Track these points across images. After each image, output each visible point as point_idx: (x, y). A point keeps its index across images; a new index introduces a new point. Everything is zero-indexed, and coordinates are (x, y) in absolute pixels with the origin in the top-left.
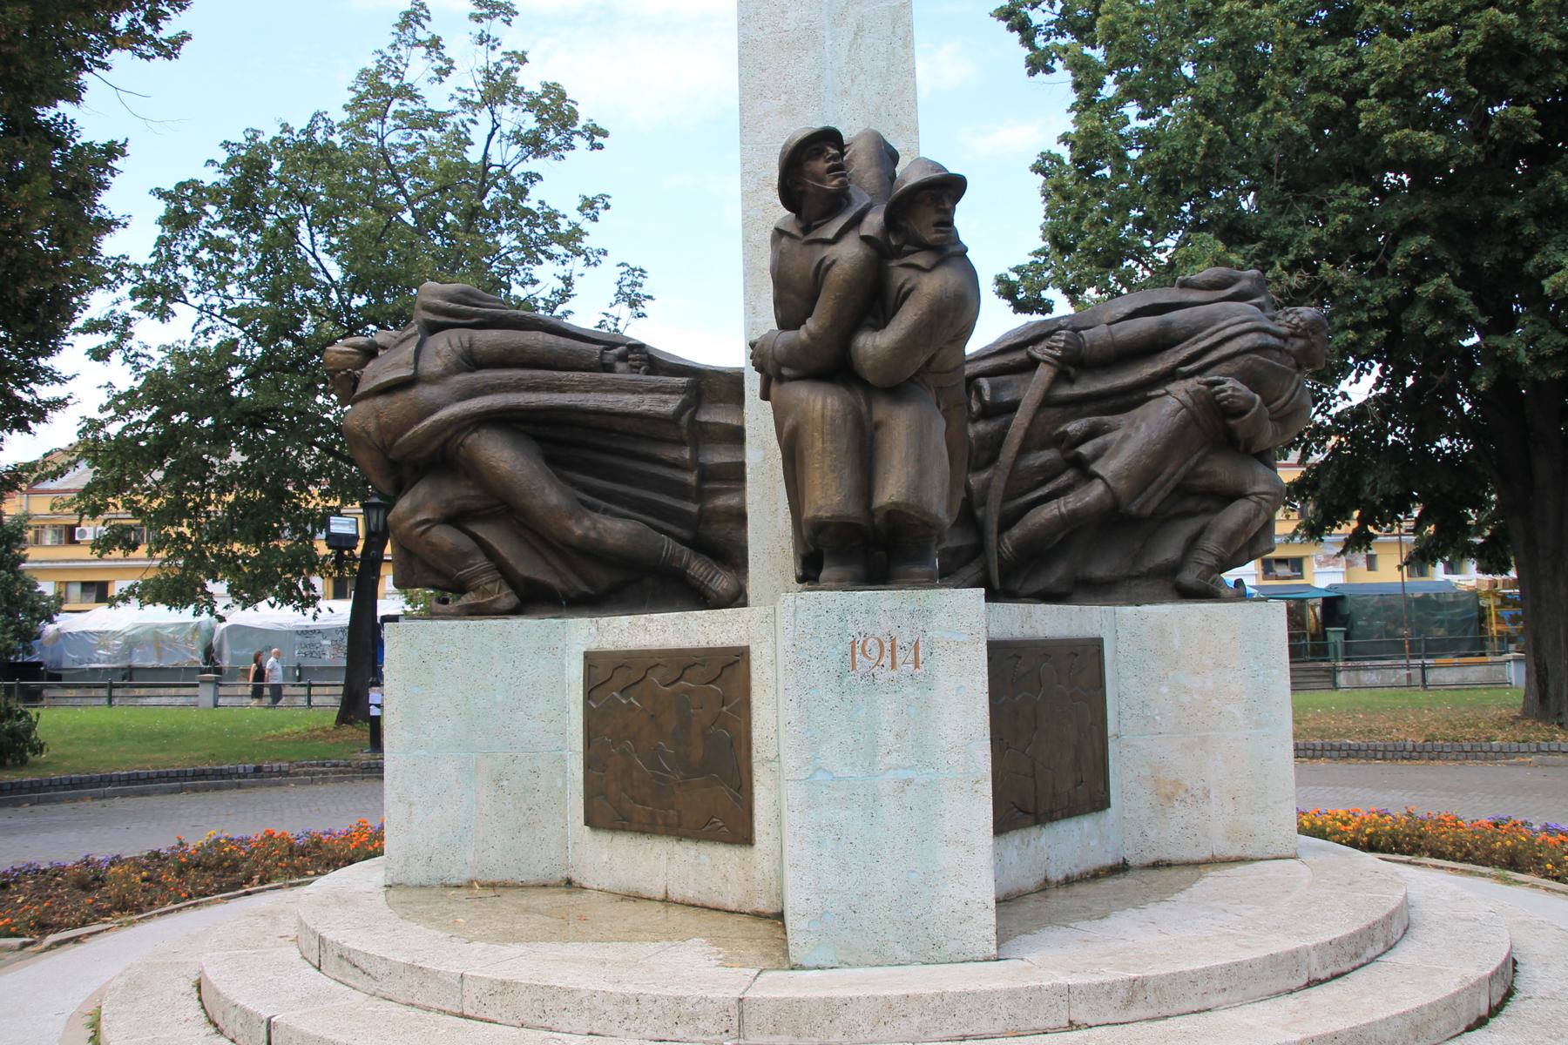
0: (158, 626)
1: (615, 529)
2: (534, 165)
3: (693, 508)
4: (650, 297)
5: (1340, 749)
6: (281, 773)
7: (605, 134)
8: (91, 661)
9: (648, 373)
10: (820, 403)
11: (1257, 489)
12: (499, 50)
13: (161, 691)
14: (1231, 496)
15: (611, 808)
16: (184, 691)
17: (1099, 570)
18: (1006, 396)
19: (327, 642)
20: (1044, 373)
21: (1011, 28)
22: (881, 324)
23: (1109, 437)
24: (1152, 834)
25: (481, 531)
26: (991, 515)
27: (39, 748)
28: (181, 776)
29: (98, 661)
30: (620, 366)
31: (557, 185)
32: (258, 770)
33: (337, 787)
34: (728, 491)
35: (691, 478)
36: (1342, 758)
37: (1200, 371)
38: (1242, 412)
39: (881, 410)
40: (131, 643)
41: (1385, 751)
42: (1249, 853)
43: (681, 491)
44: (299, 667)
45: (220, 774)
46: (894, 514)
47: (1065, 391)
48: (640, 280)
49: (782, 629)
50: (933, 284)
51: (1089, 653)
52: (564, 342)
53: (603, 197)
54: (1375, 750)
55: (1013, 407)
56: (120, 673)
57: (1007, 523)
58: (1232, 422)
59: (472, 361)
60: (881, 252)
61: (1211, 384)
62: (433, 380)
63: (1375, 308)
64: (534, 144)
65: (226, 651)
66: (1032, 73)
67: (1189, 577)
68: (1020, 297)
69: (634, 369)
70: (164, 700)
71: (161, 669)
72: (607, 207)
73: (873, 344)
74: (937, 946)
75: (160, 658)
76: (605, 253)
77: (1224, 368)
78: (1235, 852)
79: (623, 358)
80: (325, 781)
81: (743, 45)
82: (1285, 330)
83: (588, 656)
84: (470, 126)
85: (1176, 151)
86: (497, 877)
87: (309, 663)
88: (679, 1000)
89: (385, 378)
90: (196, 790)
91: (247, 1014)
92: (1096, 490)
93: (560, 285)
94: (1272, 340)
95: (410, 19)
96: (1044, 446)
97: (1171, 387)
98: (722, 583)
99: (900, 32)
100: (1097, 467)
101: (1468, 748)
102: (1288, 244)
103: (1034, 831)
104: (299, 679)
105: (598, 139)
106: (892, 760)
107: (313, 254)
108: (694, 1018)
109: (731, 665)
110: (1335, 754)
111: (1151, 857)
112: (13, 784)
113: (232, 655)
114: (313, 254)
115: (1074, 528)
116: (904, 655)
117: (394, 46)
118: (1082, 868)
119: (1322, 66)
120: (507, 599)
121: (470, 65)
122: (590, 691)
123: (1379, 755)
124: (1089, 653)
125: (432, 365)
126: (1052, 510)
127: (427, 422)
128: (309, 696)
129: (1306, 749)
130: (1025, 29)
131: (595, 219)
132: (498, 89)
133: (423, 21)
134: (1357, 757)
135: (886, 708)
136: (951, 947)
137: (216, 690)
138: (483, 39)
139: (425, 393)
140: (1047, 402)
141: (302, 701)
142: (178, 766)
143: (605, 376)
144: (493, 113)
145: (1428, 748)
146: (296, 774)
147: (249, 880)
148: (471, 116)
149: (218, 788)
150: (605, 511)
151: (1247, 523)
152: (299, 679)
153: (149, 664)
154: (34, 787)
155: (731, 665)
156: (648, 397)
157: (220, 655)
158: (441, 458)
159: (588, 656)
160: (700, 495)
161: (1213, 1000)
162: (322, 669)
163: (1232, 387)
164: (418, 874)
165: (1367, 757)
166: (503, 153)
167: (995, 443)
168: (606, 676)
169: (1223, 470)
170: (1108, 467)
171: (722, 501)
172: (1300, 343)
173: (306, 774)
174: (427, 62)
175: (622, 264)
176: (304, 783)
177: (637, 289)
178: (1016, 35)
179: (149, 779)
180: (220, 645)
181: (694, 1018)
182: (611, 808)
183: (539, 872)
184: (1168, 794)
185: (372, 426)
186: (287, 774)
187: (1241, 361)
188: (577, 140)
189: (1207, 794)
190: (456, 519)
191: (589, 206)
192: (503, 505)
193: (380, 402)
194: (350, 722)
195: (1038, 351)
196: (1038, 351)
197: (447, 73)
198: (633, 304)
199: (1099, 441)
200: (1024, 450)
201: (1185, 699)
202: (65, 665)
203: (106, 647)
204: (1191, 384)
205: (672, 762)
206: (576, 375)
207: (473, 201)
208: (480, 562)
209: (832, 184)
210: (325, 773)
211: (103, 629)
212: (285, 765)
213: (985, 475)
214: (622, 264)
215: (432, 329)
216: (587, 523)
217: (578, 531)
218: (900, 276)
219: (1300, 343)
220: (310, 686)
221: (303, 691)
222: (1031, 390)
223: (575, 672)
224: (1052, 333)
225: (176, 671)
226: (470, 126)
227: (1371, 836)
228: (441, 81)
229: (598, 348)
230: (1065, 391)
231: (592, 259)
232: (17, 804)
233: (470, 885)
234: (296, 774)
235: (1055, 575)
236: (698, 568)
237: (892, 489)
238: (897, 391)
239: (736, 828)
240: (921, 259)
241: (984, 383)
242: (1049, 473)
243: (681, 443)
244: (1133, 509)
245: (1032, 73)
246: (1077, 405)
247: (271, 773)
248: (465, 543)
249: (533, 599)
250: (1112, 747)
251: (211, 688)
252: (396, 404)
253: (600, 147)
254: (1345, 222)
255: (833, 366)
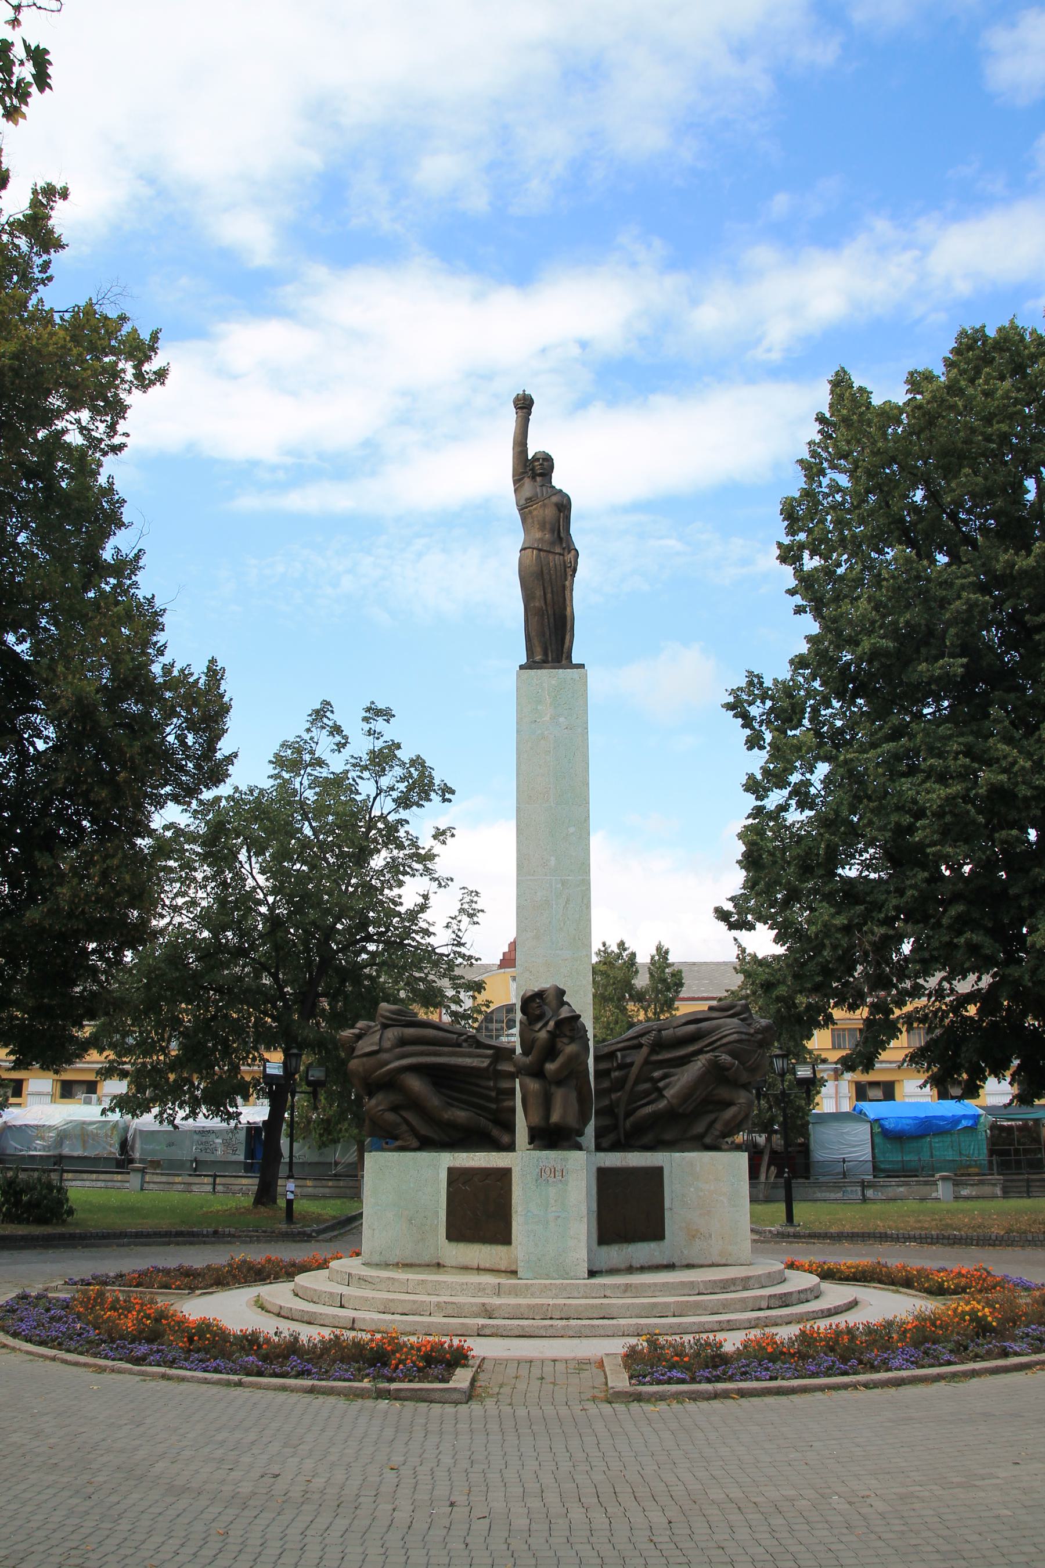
0: (84, 1123)
1: (461, 1115)
2: (403, 814)
3: (494, 1106)
4: (482, 911)
5: (949, 1238)
6: (230, 1235)
7: (453, 792)
8: (30, 1149)
9: (476, 1048)
10: (534, 1085)
11: (742, 1101)
12: (382, 739)
13: (85, 1176)
14: (730, 1104)
15: (457, 1233)
16: (102, 1177)
17: (668, 1136)
18: (628, 1060)
19: (219, 1141)
20: (645, 1050)
21: (735, 716)
22: (553, 1060)
23: (672, 1079)
24: (686, 1252)
25: (404, 1114)
26: (621, 1112)
27: (71, 1212)
28: (168, 1234)
29: (35, 1149)
30: (464, 1044)
31: (420, 824)
32: (216, 1232)
33: (265, 1245)
34: (508, 1099)
35: (493, 1094)
36: (950, 1245)
37: (712, 1050)
38: (728, 1069)
39: (553, 1089)
40: (63, 1135)
41: (978, 1240)
42: (729, 1262)
43: (489, 1099)
44: (196, 1160)
45: (192, 1234)
46: (556, 1125)
47: (655, 1058)
48: (475, 899)
49: (522, 1161)
50: (570, 1049)
51: (656, 1174)
52: (441, 1034)
53: (449, 828)
54: (972, 1239)
55: (632, 1064)
56: (52, 1160)
57: (628, 1114)
58: (726, 1073)
59: (403, 1042)
60: (553, 1035)
61: (716, 1057)
62: (387, 1051)
63: (934, 949)
64: (404, 802)
65: (138, 1145)
66: (750, 749)
67: (708, 1140)
68: (732, 920)
69: (470, 1046)
70: (87, 1184)
71: (85, 1157)
72: (453, 835)
73: (550, 1067)
74: (567, 1274)
75: (85, 1148)
76: (452, 880)
77: (722, 1049)
78: (723, 1261)
79: (465, 1040)
80: (259, 1241)
81: (518, 908)
82: (752, 1031)
83: (449, 1169)
84: (358, 780)
85: (810, 848)
86: (408, 1261)
87: (203, 1157)
88: (480, 1284)
89: (368, 1050)
90: (178, 1244)
91: (331, 1294)
92: (662, 1104)
93: (421, 900)
94: (744, 1037)
95: (319, 715)
96: (645, 1081)
97: (700, 1057)
98: (505, 1139)
99: (585, 901)
100: (665, 1093)
101: (1030, 1238)
102: (882, 905)
103: (625, 1245)
104: (195, 1170)
105: (447, 796)
106: (553, 1209)
107: (251, 874)
108: (484, 1289)
109: (504, 1175)
110: (946, 1241)
111: (685, 1262)
112: (70, 1234)
113: (142, 1148)
114: (251, 874)
115: (657, 1118)
116: (558, 1174)
117: (308, 730)
118: (650, 1264)
119: (901, 793)
120: (415, 1143)
121: (361, 746)
122: (450, 1183)
123: (975, 1242)
124: (659, 1171)
125: (387, 1044)
126: (649, 1109)
127: (384, 1069)
128: (214, 1184)
129: (926, 1238)
130: (747, 721)
131: (444, 843)
132: (381, 759)
133: (328, 714)
134: (960, 1244)
135: (552, 1191)
136: (572, 1274)
137: (143, 1178)
138: (370, 733)
139: (385, 1056)
140: (646, 1062)
141: (210, 1188)
142: (165, 1228)
143: (458, 1049)
144: (377, 782)
145: (1005, 1238)
146: (240, 1236)
147: (269, 1277)
148: (359, 773)
149: (192, 1243)
150: (457, 1107)
151: (734, 1117)
152: (195, 1170)
153: (75, 1154)
154: (62, 1237)
155: (504, 1175)
156: (476, 1060)
157: (133, 1148)
158: (390, 1083)
159: (449, 1169)
160: (496, 1100)
161: (657, 1294)
162: (214, 1163)
163: (725, 1058)
164: (376, 1259)
165: (966, 1244)
166: (383, 806)
167: (623, 1081)
168: (456, 1176)
169: (724, 1093)
170: (669, 1093)
171: (506, 1104)
172: (760, 1036)
173: (246, 1236)
174: (331, 737)
175: (464, 888)
176: (245, 1242)
177: (474, 906)
178: (740, 721)
179: (148, 1235)
180: (134, 1139)
181: (484, 1289)
182: (457, 1233)
183: (426, 1258)
184: (693, 1235)
185: (361, 1069)
186: (234, 1236)
187: (729, 1046)
188: (433, 795)
189: (710, 1236)
190: (395, 1109)
191: (439, 835)
192: (414, 1104)
193: (365, 1059)
194: (263, 1204)
195: (643, 1040)
196: (643, 1040)
197: (344, 745)
198: (471, 916)
199: (667, 1080)
200: (637, 1082)
201: (701, 1194)
202: (8, 1152)
203: (42, 1138)
204: (708, 1056)
205: (480, 1213)
206: (446, 1049)
207: (355, 833)
208: (404, 1127)
209: (538, 1012)
210: (258, 1237)
211: (40, 1123)
212: (233, 1230)
213: (619, 1094)
214: (464, 888)
215: (385, 1026)
216: (450, 1113)
217: (446, 1116)
218: (559, 1045)
219: (760, 1036)
220: (215, 1176)
221: (211, 1180)
222: (638, 1058)
223: (444, 1176)
224: (650, 1032)
225: (96, 1160)
226: (358, 780)
227: (854, 1273)
228: (340, 752)
229: (455, 1036)
230: (655, 1058)
231: (442, 883)
232: (74, 1247)
233: (397, 1264)
234: (240, 1236)
235: (647, 1139)
236: (495, 1132)
237: (555, 1118)
238: (559, 1083)
239: (504, 1237)
240: (565, 1040)
241: (619, 1054)
242: (647, 1093)
243: (489, 1079)
244: (681, 1111)
245: (750, 749)
246: (661, 1064)
247: (224, 1235)
248: (399, 1120)
249: (426, 1144)
250: (667, 1214)
251: (139, 1175)
252: (371, 1061)
253: (450, 801)
254: (913, 896)
255: (538, 1073)
